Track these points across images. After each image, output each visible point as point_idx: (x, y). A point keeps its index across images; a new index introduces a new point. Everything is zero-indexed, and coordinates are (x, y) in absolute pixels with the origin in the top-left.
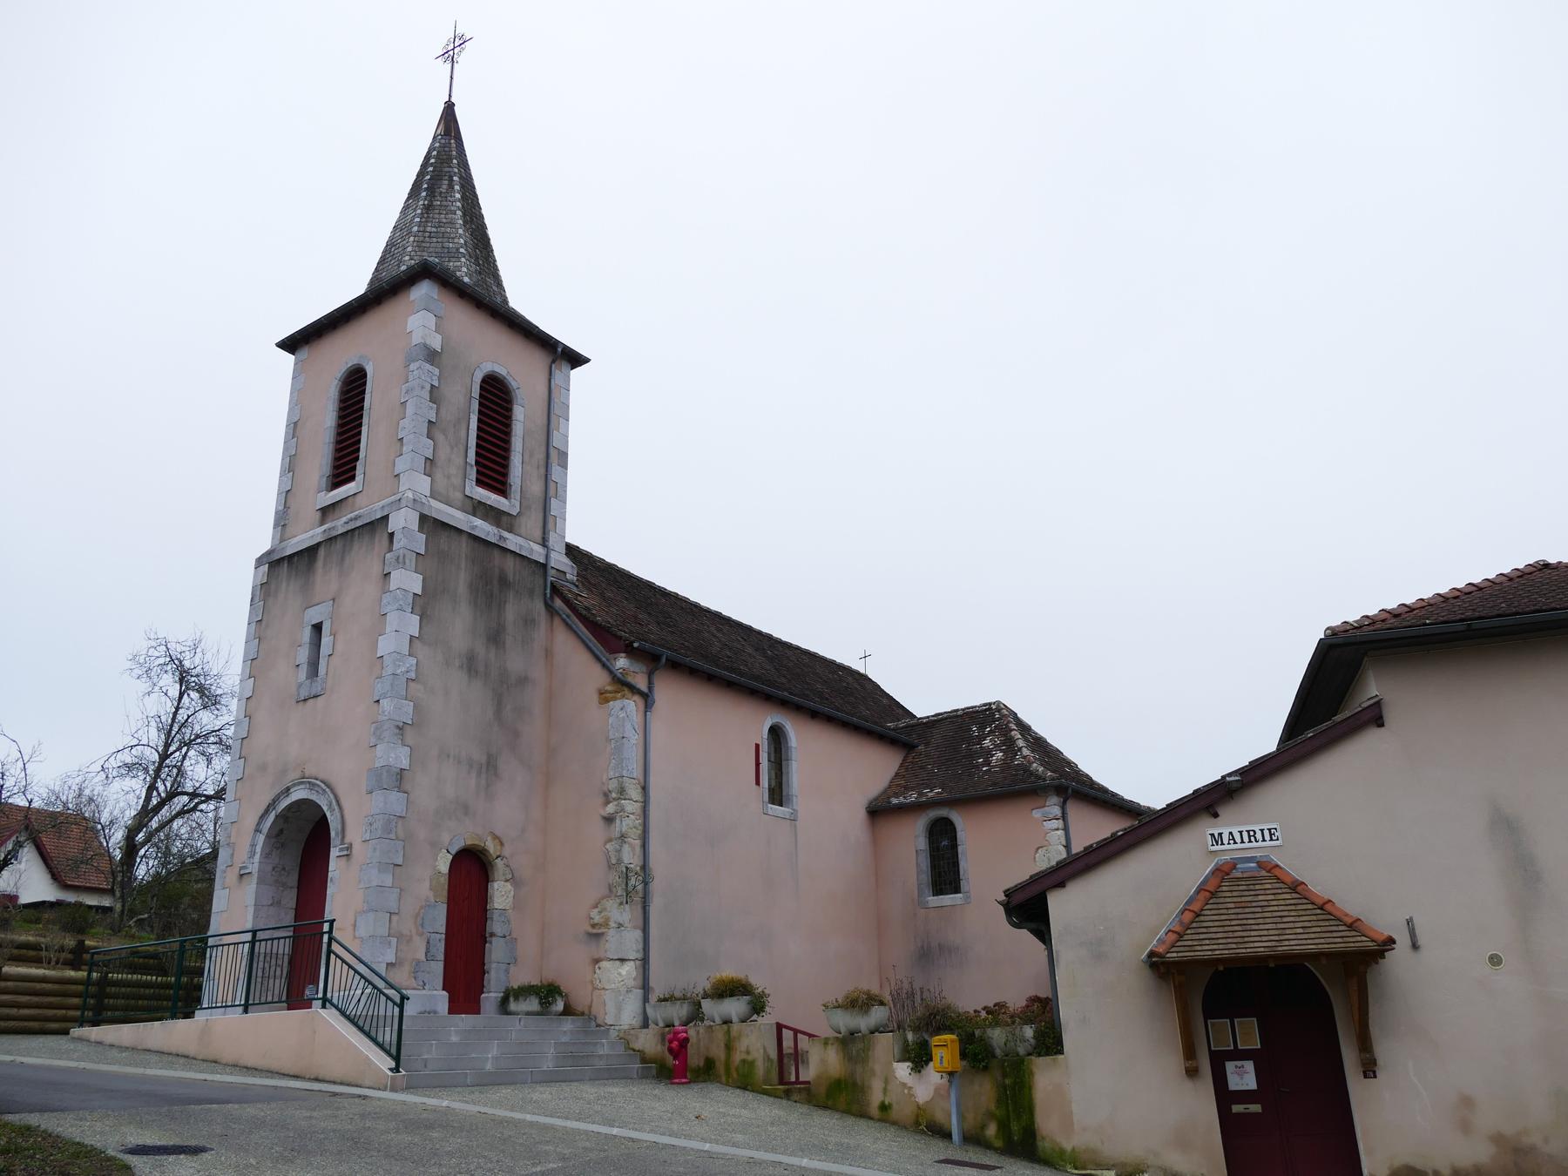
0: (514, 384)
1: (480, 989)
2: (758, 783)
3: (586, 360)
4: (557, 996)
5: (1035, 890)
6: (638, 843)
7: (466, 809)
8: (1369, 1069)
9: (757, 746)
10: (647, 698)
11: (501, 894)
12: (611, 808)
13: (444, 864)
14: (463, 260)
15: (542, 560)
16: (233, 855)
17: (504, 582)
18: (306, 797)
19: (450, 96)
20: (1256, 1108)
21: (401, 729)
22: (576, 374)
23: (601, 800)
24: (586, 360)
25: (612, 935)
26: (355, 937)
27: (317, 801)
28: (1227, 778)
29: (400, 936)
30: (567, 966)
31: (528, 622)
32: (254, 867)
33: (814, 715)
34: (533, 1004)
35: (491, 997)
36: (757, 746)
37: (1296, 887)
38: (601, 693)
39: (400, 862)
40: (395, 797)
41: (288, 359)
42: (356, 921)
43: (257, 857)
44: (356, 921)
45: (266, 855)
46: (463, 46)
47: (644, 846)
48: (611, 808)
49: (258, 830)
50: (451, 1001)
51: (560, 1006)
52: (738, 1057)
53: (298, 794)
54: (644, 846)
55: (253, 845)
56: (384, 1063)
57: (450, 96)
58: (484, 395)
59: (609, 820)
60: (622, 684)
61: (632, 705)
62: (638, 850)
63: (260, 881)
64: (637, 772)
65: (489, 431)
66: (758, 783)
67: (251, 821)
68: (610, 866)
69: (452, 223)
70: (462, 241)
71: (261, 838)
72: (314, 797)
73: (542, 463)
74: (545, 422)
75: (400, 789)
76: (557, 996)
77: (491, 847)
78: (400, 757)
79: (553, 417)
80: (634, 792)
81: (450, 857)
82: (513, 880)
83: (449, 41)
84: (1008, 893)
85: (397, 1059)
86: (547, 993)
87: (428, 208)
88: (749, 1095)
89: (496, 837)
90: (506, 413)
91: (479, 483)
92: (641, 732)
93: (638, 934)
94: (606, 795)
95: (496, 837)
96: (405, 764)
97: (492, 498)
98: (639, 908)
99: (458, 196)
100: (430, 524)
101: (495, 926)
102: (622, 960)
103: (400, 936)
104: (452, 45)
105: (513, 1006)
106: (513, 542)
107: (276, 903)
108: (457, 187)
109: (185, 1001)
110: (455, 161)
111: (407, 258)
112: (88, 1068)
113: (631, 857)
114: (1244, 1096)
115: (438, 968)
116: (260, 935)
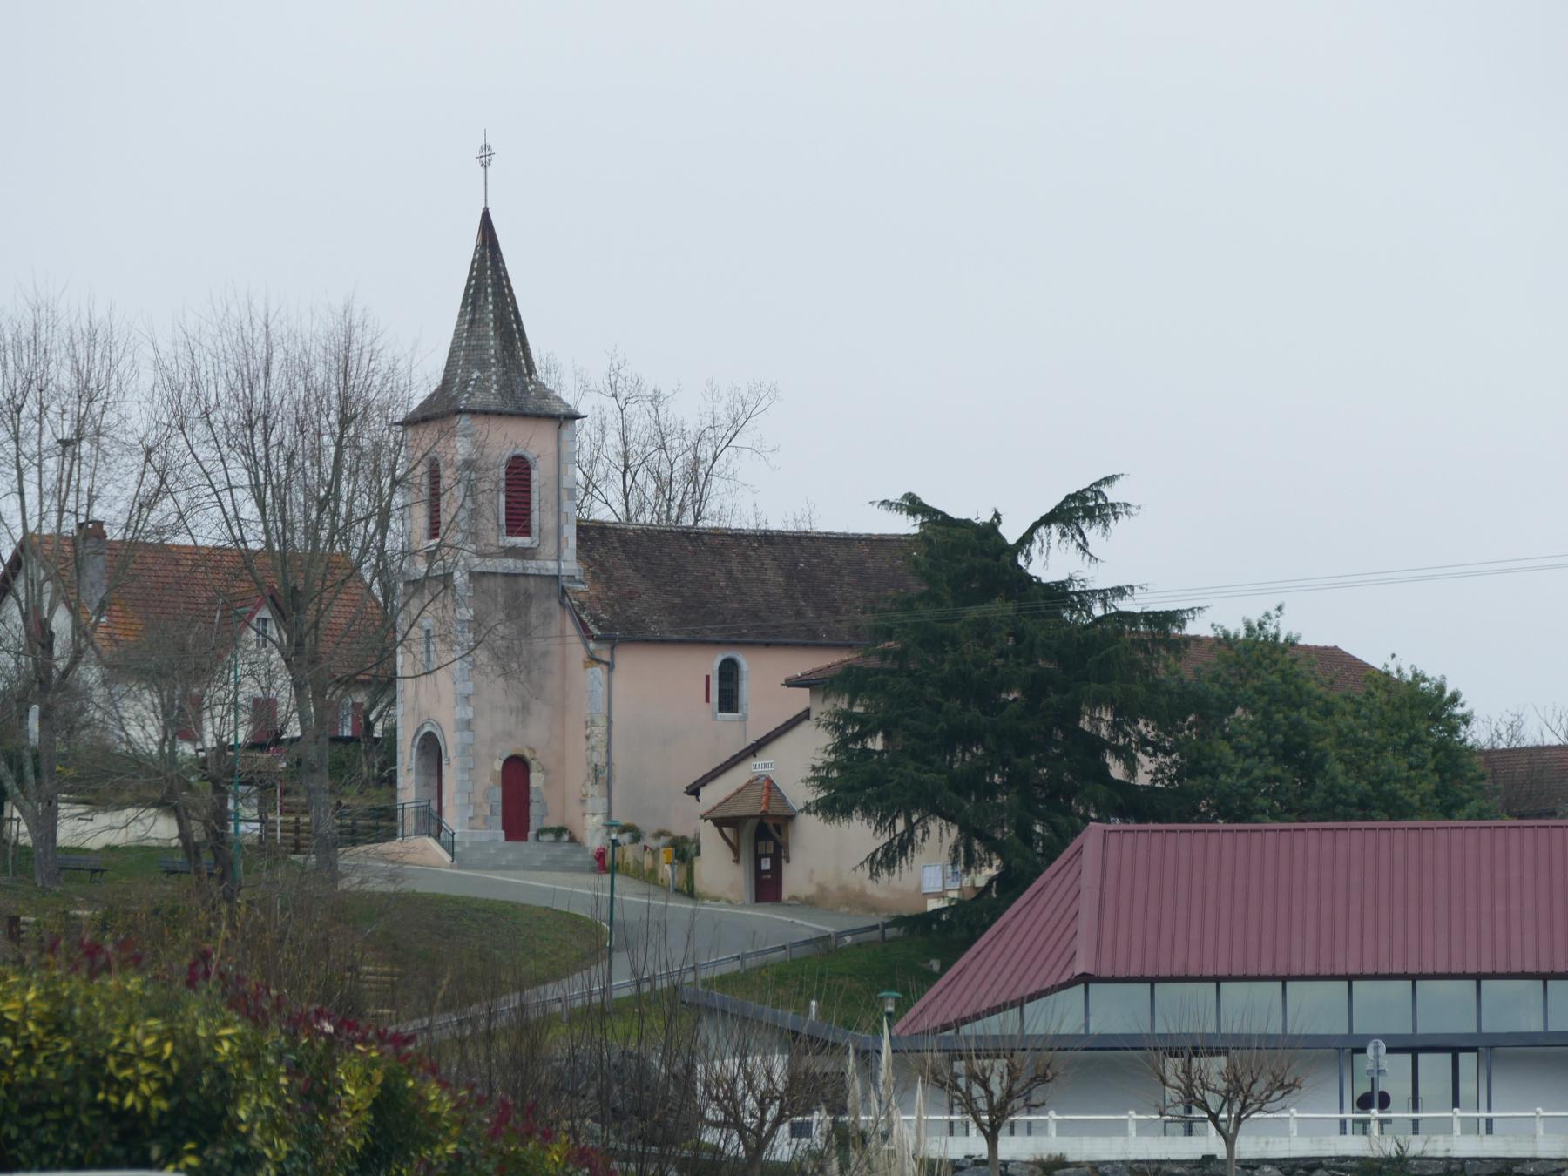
1: (528, 830)
2: (708, 700)
4: (903, 814)
5: (697, 785)
6: (604, 750)
7: (510, 735)
8: (788, 861)
9: (708, 678)
10: (610, 666)
11: (536, 780)
12: (588, 731)
13: (498, 766)
14: (493, 369)
15: (556, 573)
17: (529, 597)
20: (769, 877)
21: (467, 698)
23: (584, 725)
25: (589, 801)
29: (475, 804)
30: (572, 818)
31: (547, 616)
32: (413, 766)
34: (551, 837)
35: (532, 833)
36: (708, 678)
37: (739, 791)
38: (585, 662)
39: (471, 766)
40: (466, 734)
43: (414, 761)
45: (419, 759)
47: (608, 752)
48: (588, 731)
49: (413, 746)
50: (506, 835)
51: (566, 837)
52: (625, 861)
53: (428, 728)
54: (608, 752)
55: (411, 754)
56: (448, 858)
59: (587, 738)
60: (593, 660)
61: (599, 671)
62: (604, 754)
63: (417, 773)
64: (601, 706)
66: (708, 700)
68: (588, 764)
69: (486, 335)
70: (493, 352)
71: (415, 750)
72: (433, 730)
73: (555, 503)
74: (556, 473)
75: (469, 730)
76: (903, 814)
77: (527, 754)
78: (469, 713)
79: (563, 466)
80: (602, 721)
81: (501, 762)
82: (543, 770)
84: (687, 788)
85: (453, 855)
86: (559, 831)
87: (472, 322)
88: (629, 879)
89: (530, 749)
92: (605, 685)
93: (605, 800)
94: (586, 723)
95: (530, 749)
96: (470, 715)
97: (520, 541)
98: (605, 787)
99: (491, 307)
100: (475, 576)
101: (533, 796)
102: (594, 814)
103: (475, 804)
105: (541, 838)
106: (532, 567)
107: (426, 785)
108: (490, 299)
109: (391, 835)
110: (489, 272)
111: (459, 371)
112: (1072, 1157)
113: (598, 758)
114: (766, 872)
115: (498, 819)
116: (406, 806)
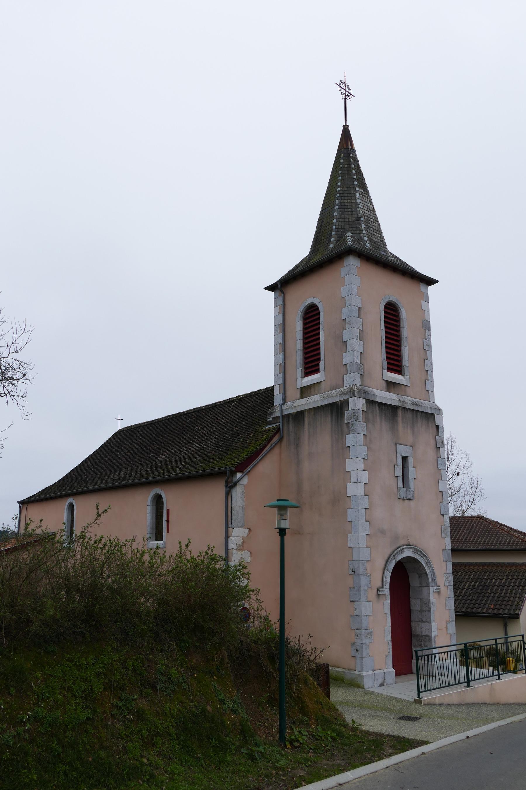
0: (395, 300)
3: (436, 282)
9: (168, 531)
16: (370, 581)
18: (412, 556)
19: (346, 121)
22: (431, 288)
24: (436, 282)
26: (447, 633)
27: (419, 560)
28: (343, 763)
33: (82, 493)
36: (168, 531)
41: (271, 294)
42: (447, 626)
44: (447, 626)
46: (346, 85)
53: (408, 553)
57: (346, 121)
58: (386, 311)
65: (394, 334)
67: (380, 563)
72: (417, 557)
83: (350, 90)
90: (397, 324)
91: (390, 370)
104: (343, 90)
